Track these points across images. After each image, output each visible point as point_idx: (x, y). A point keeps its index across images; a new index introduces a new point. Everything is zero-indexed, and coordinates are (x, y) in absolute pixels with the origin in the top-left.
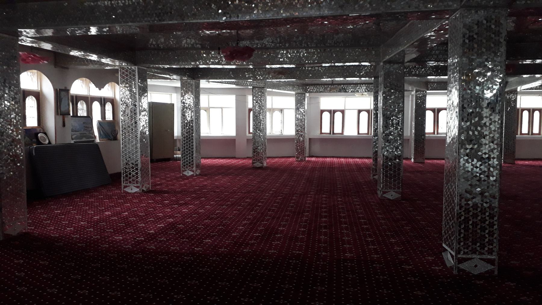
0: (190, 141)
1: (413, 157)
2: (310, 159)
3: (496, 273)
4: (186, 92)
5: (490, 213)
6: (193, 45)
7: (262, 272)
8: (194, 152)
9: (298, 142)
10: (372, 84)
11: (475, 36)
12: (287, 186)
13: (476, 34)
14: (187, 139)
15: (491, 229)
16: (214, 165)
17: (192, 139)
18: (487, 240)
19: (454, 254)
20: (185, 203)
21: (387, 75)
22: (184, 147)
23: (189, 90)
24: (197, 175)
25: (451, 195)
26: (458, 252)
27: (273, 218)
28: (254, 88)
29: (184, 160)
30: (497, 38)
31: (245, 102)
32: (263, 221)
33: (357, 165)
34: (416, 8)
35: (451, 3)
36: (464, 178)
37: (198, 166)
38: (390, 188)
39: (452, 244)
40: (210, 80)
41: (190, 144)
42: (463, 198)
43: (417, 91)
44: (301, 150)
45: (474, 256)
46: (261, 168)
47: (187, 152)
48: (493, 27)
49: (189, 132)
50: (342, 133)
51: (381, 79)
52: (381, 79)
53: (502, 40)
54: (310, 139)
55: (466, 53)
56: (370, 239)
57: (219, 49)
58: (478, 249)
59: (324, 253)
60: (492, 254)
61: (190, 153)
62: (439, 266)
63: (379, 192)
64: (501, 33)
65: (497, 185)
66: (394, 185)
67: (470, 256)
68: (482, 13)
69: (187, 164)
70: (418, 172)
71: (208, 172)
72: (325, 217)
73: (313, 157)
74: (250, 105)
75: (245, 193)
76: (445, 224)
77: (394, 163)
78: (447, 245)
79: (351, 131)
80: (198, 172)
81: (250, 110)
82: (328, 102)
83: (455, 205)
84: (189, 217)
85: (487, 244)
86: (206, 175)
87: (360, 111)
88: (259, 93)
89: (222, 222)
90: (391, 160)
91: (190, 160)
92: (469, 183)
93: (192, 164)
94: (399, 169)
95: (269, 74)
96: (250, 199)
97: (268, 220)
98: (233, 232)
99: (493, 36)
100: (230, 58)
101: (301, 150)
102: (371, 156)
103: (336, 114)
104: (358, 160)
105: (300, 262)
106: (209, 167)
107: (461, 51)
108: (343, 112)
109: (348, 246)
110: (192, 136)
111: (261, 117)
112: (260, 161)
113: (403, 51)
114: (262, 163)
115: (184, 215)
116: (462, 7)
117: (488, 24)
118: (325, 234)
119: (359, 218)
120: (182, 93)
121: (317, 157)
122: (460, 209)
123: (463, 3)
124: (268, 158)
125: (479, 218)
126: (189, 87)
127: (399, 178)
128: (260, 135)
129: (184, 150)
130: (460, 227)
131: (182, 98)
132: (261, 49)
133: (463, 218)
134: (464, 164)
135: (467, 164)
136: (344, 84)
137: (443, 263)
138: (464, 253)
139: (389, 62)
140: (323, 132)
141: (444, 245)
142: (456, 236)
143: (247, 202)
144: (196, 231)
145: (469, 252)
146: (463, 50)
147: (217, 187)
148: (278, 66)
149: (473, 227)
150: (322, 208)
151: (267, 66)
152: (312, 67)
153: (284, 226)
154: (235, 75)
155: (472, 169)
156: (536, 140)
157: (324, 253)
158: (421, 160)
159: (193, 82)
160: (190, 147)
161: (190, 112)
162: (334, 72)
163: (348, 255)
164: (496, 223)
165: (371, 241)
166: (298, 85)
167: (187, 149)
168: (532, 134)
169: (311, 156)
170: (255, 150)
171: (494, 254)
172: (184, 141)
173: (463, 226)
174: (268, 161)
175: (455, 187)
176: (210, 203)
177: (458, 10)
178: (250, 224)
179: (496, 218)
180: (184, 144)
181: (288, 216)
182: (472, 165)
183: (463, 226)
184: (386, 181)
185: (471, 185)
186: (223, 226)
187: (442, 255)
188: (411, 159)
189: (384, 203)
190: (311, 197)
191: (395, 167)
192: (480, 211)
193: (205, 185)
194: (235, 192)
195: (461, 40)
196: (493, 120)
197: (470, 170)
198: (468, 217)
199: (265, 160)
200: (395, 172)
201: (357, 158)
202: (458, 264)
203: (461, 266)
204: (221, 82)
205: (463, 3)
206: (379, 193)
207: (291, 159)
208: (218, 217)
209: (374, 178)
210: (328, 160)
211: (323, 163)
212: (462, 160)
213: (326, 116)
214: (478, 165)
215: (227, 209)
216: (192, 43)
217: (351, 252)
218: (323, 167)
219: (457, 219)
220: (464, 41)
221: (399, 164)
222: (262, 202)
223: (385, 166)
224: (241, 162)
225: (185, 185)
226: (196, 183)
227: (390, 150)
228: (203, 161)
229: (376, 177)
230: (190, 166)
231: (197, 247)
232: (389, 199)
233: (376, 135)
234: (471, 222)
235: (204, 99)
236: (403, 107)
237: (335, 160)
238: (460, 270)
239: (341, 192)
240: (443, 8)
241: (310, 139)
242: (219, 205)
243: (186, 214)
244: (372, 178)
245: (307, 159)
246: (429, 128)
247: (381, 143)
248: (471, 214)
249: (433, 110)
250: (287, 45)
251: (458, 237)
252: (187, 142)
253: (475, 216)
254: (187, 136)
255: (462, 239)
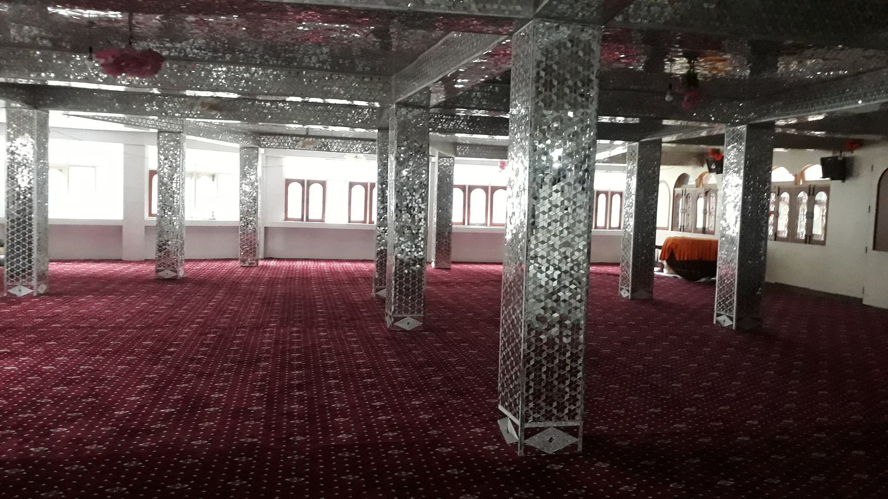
0: (24, 228)
1: (433, 260)
2: (266, 263)
3: (580, 448)
4: (19, 133)
5: (572, 353)
6: (34, 38)
7: (179, 486)
8: (35, 250)
9: (246, 233)
10: (374, 140)
11: (555, 67)
12: (225, 313)
13: (557, 63)
14: (19, 225)
15: (574, 379)
16: (78, 274)
17: (31, 225)
18: (567, 397)
19: (518, 422)
20: (12, 352)
21: (403, 127)
22: (12, 240)
23: (25, 129)
24: (39, 295)
25: (514, 326)
26: (525, 420)
27: (200, 375)
28: (160, 132)
29: (12, 264)
30: (587, 73)
31: (143, 158)
32: (179, 382)
33: (347, 273)
34: (465, 9)
35: (519, 8)
36: (535, 297)
37: (42, 277)
38: (406, 311)
39: (516, 405)
40: (71, 113)
41: (24, 234)
42: (533, 329)
43: (440, 157)
44: (250, 248)
45: (549, 424)
46: (173, 280)
47: (18, 249)
48: (581, 54)
49: (24, 210)
50: (322, 221)
51: (392, 134)
52: (392, 134)
53: (593, 77)
54: (266, 228)
55: (540, 93)
56: (378, 403)
57: (91, 50)
58: (555, 411)
59: (299, 438)
60: (573, 418)
61: (24, 252)
62: (494, 444)
63: (387, 319)
64: (592, 66)
65: (583, 308)
66: (413, 307)
67: (541, 425)
68: (565, 32)
69: (18, 274)
70: (443, 283)
71: (61, 288)
72: (299, 368)
73: (271, 259)
74: (153, 164)
75: (142, 328)
76: (503, 372)
77: (413, 271)
78: (506, 408)
79: (336, 218)
80: (43, 288)
81: (152, 173)
82: (298, 164)
83: (520, 341)
84: (19, 382)
85: (567, 404)
86: (59, 295)
87: (351, 185)
88: (171, 141)
89: (93, 389)
90: (408, 265)
91: (24, 265)
92: (543, 304)
93: (30, 274)
94: (420, 281)
95: (191, 107)
96: (152, 340)
97: (188, 381)
98: (119, 409)
99: (580, 69)
100: (115, 68)
101: (250, 248)
102: (373, 256)
103: (312, 187)
104: (348, 264)
105: (254, 459)
106: (65, 278)
107: (534, 89)
108: (323, 184)
109: (342, 419)
110: (30, 219)
111: (174, 185)
112: (173, 267)
113: (427, 88)
114: (176, 272)
115: (8, 377)
116: (537, 16)
117: (574, 49)
118: (301, 400)
119: (358, 366)
120: (9, 134)
121: (279, 259)
122: (529, 348)
123: (538, 10)
124: (187, 261)
125: (557, 361)
126: (25, 123)
127: (420, 296)
128: (171, 220)
129: (13, 246)
130: (528, 376)
131: (9, 144)
132: (176, 59)
133: (532, 362)
134: (535, 275)
135: (539, 275)
136: (326, 137)
137: (500, 438)
138: (535, 420)
139: (405, 104)
140: (289, 216)
141: (501, 408)
142: (523, 393)
143: (145, 347)
144: (34, 412)
145: (542, 419)
146: (537, 88)
147: (82, 318)
148: (210, 94)
149: (547, 377)
150: (291, 351)
151: (189, 93)
152: (272, 102)
153: (222, 390)
154: (125, 103)
155: (547, 283)
156: (601, 236)
157: (299, 438)
158: (446, 265)
159: (32, 113)
160: (24, 240)
161: (26, 171)
162: (306, 113)
163: (343, 436)
164: (580, 368)
165: (380, 406)
166: (245, 133)
167: (18, 243)
168: (610, 228)
169: (266, 259)
170: (161, 248)
171: (578, 418)
172: (13, 227)
173: (532, 376)
174: (187, 266)
175: (521, 312)
176: (66, 351)
177: (529, 20)
178: (154, 389)
179: (580, 361)
180: (13, 234)
181: (229, 369)
182: (547, 276)
183: (532, 376)
184: (400, 299)
185: (544, 308)
186: (96, 396)
187: (498, 425)
188: (430, 263)
189: (397, 337)
190: (271, 332)
191: (414, 277)
192: (557, 351)
193: (58, 315)
194: (121, 328)
195: (535, 72)
196: (574, 207)
197: (543, 283)
198: (541, 361)
199: (182, 265)
200: (414, 285)
201: (347, 261)
202: (525, 439)
203: (529, 442)
204: (93, 118)
205: (538, 10)
206: (389, 321)
207: (231, 264)
208: (85, 379)
209: (377, 295)
210: (299, 264)
211: (290, 270)
212: (531, 267)
213: (295, 190)
214: (556, 276)
215: (104, 362)
216: (32, 34)
217: (348, 432)
218: (290, 278)
219: (524, 365)
220: (538, 73)
221: (420, 272)
222: (177, 346)
223: (399, 275)
224: (132, 269)
225: (13, 315)
226: (38, 311)
227: (407, 250)
228: (54, 267)
229: (383, 293)
230: (24, 277)
231: (36, 445)
232: (403, 330)
233: (383, 221)
234: (544, 369)
235: (54, 144)
236: (427, 180)
237: (311, 265)
238: (527, 448)
239: (324, 322)
240: (507, 14)
241: (266, 228)
242: (88, 354)
243: (12, 375)
244: (373, 294)
245: (261, 263)
246: (457, 216)
247: (392, 237)
248: (544, 355)
249: (463, 188)
250: (228, 57)
251: (526, 394)
252: (18, 231)
253: (551, 358)
254: (18, 219)
255: (531, 398)
